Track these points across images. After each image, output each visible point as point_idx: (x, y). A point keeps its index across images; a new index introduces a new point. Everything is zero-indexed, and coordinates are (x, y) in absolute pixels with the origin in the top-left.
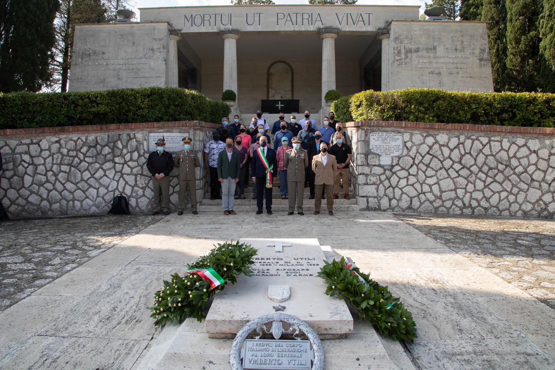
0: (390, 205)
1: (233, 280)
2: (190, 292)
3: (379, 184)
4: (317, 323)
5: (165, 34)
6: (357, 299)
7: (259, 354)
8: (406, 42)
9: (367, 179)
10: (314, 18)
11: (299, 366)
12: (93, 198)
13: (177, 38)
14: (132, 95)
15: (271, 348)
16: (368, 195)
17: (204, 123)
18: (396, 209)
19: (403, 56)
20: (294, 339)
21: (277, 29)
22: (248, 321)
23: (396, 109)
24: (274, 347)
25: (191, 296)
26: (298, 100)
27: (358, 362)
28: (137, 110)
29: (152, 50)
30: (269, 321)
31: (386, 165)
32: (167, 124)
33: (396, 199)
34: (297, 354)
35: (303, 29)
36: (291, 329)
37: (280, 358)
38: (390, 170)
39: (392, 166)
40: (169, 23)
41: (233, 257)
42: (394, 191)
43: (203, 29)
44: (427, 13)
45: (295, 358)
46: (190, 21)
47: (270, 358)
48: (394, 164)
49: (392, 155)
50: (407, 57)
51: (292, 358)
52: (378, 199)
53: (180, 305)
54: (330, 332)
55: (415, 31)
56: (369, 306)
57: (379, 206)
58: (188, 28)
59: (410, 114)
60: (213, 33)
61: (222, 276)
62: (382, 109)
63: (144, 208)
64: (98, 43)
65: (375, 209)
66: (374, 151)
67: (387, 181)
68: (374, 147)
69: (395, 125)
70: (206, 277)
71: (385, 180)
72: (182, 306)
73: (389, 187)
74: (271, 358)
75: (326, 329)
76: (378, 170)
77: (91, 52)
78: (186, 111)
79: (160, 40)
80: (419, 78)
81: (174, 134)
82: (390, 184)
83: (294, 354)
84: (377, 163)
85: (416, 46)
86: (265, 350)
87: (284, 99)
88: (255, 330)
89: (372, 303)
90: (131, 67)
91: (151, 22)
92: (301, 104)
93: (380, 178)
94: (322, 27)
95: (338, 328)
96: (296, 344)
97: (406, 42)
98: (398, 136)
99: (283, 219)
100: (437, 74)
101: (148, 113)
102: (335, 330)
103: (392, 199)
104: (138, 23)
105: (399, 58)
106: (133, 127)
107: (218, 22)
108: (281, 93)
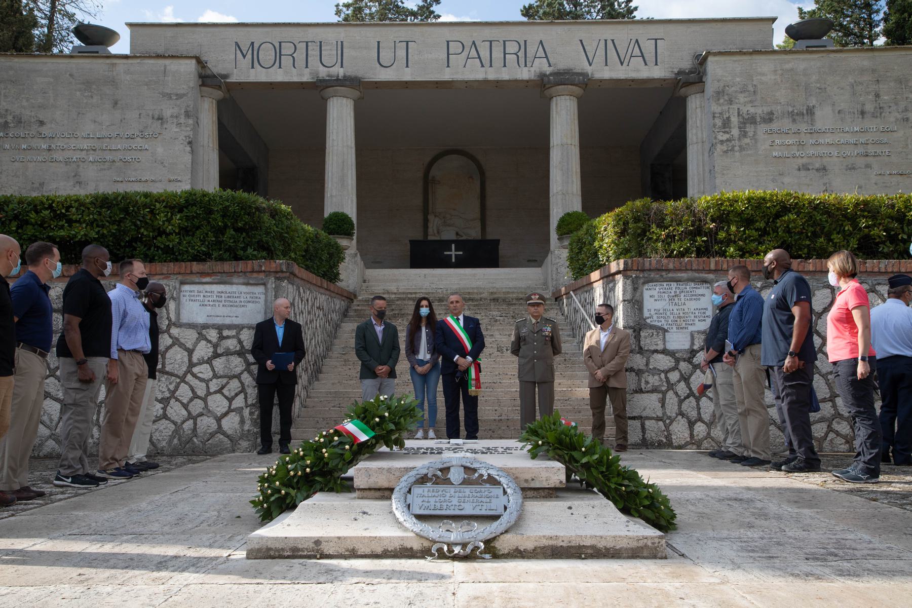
0: (692, 435)
3: (667, 391)
4: (514, 471)
5: (192, 84)
6: (575, 454)
7: (432, 500)
8: (742, 100)
9: (639, 380)
10: (531, 51)
12: (51, 420)
13: (219, 94)
14: (145, 206)
16: (644, 414)
18: (705, 444)
19: (735, 132)
21: (447, 75)
23: (700, 234)
24: (452, 493)
26: (497, 242)
27: (571, 511)
28: (155, 238)
29: (160, 118)
30: (445, 466)
31: (678, 351)
33: (703, 422)
34: (484, 500)
35: (505, 75)
36: (476, 475)
38: (689, 361)
39: (693, 352)
40: (199, 61)
42: (698, 405)
43: (278, 76)
44: (791, 31)
46: (249, 56)
48: (695, 348)
49: (691, 328)
50: (744, 134)
52: (664, 422)
54: (533, 485)
55: (763, 74)
57: (669, 437)
58: (244, 73)
59: (728, 246)
60: (302, 83)
61: (373, 430)
62: (668, 236)
63: (164, 444)
64: (27, 100)
65: (660, 445)
66: (654, 321)
68: (653, 312)
70: (348, 433)
71: (679, 381)
73: (687, 397)
75: (526, 481)
76: (663, 362)
77: (9, 118)
78: (258, 242)
79: (180, 96)
80: (773, 181)
81: (234, 288)
82: (690, 389)
83: (480, 499)
84: (660, 347)
85: (766, 109)
87: (464, 238)
88: (426, 475)
89: (596, 456)
90: (108, 158)
91: (159, 57)
92: (503, 249)
93: (667, 378)
94: (548, 70)
97: (742, 100)
98: (702, 290)
100: (817, 170)
101: (179, 243)
103: (696, 421)
104: (126, 57)
105: (726, 137)
107: (314, 61)
108: (456, 223)
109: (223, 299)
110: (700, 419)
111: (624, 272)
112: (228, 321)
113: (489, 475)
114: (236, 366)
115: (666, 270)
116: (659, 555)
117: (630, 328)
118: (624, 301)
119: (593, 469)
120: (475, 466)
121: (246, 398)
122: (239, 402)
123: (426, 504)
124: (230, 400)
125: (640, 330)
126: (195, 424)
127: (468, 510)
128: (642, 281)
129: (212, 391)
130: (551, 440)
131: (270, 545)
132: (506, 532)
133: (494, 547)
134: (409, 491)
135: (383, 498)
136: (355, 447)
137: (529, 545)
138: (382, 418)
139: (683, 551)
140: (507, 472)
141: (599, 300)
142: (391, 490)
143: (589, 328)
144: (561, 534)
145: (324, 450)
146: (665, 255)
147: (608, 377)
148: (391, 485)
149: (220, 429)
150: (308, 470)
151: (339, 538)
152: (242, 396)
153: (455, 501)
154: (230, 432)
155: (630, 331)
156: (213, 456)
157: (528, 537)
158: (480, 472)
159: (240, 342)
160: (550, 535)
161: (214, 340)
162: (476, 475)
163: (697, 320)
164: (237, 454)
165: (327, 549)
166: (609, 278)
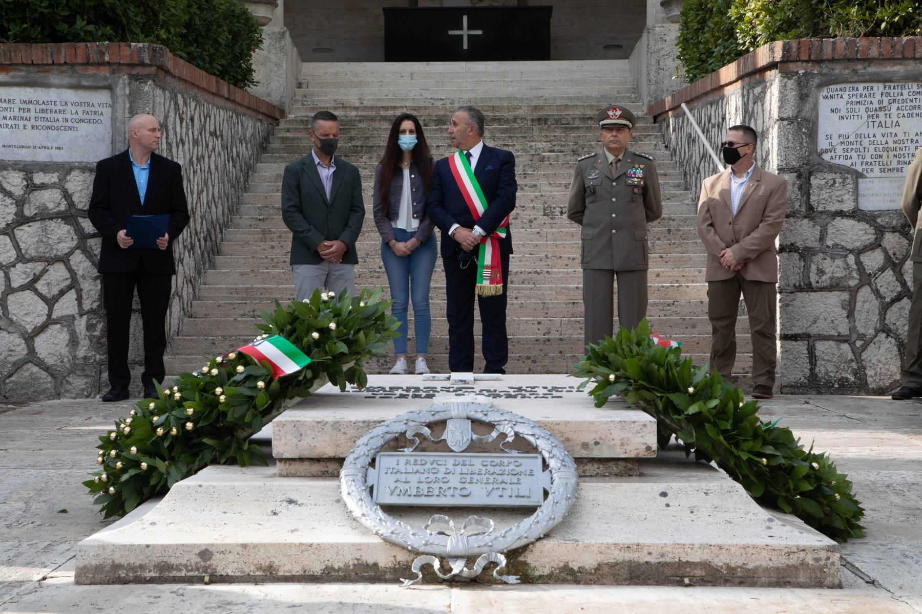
2: (219, 390)
4: (562, 428)
7: (414, 479)
9: (807, 268)
16: (814, 330)
17: (169, 59)
20: (502, 451)
25: (222, 398)
27: (665, 500)
30: (437, 417)
31: (881, 213)
36: (494, 434)
37: (467, 486)
45: (503, 485)
47: (442, 485)
51: (495, 486)
54: (596, 453)
57: (860, 372)
61: (308, 353)
65: (844, 388)
67: (889, 273)
68: (835, 141)
70: (263, 358)
71: (882, 270)
72: (195, 430)
73: (898, 299)
75: (585, 446)
76: (853, 233)
81: (53, 94)
83: (500, 478)
84: (848, 206)
88: (403, 434)
89: (714, 403)
93: (859, 263)
95: (618, 443)
96: (506, 461)
102: (610, 447)
111: (782, 65)
112: (42, 156)
113: (517, 434)
114: (60, 240)
116: (828, 581)
117: (791, 170)
119: (707, 425)
120: (491, 418)
121: (79, 299)
122: (67, 306)
123: (402, 486)
124: (51, 302)
125: (810, 174)
127: (479, 497)
128: (817, 81)
129: (15, 285)
130: (631, 372)
132: (547, 536)
133: (525, 564)
134: (372, 463)
137: (589, 561)
138: (324, 331)
139: (873, 575)
140: (550, 429)
142: (340, 461)
145: (219, 390)
148: (339, 453)
149: (32, 356)
150: (189, 425)
151: (245, 546)
152: (72, 295)
153: (455, 481)
154: (50, 361)
157: (587, 546)
159: (67, 196)
160: (627, 542)
161: (18, 191)
162: (494, 434)
164: (65, 400)
165: (224, 566)
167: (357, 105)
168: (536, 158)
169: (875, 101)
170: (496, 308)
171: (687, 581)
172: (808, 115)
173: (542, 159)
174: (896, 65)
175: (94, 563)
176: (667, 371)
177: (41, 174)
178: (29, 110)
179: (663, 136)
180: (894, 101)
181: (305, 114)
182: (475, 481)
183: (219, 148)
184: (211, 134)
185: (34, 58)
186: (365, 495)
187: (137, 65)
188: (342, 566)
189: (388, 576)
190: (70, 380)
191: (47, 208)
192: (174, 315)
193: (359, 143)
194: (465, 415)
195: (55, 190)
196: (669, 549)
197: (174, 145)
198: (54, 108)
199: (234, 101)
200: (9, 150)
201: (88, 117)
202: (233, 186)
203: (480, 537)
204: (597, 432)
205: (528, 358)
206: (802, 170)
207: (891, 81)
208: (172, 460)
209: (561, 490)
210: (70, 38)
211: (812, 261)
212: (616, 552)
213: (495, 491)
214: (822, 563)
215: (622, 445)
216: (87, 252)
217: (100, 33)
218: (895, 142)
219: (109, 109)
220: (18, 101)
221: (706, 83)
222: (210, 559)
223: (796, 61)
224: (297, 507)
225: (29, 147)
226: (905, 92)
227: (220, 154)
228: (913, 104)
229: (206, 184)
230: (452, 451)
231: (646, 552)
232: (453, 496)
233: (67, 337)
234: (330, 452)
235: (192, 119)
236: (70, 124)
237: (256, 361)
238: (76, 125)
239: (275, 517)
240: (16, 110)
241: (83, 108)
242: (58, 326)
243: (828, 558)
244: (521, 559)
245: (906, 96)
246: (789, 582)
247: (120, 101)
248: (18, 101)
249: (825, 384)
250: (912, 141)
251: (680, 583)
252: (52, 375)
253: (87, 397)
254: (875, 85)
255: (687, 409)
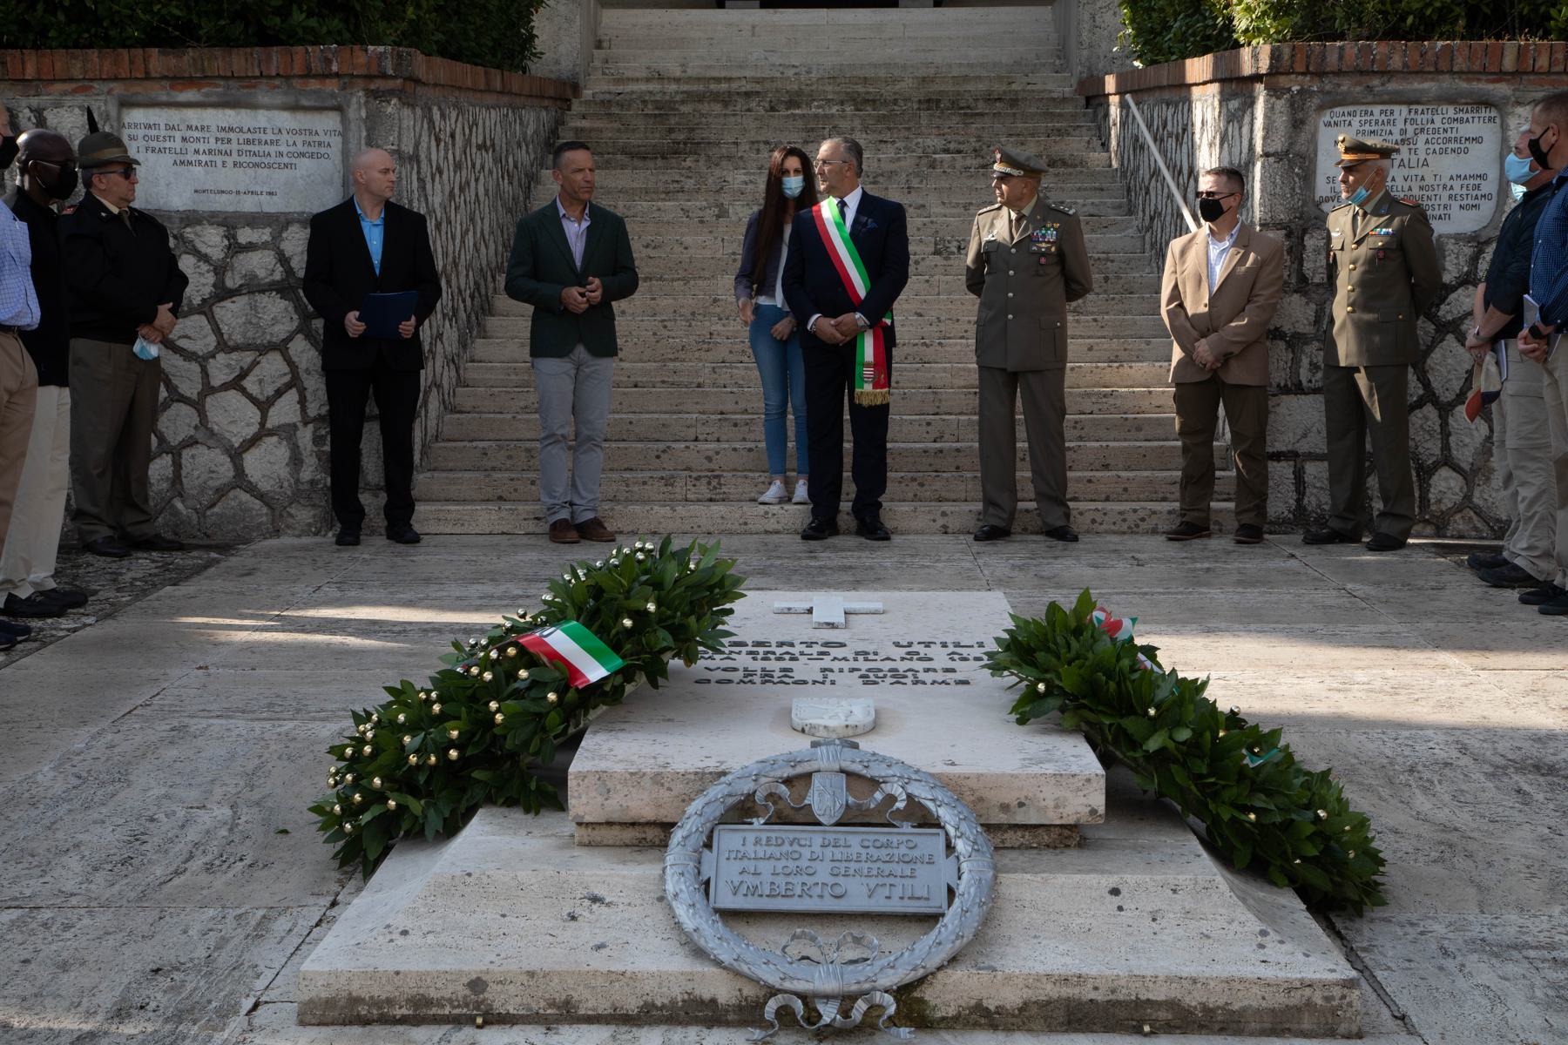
1: (656, 672)
4: (972, 783)
6: (1130, 724)
7: (766, 867)
9: (1296, 362)
11: (906, 902)
15: (806, 853)
16: (1303, 447)
17: (420, 63)
18: (1458, 523)
22: (724, 774)
24: (817, 848)
25: (499, 717)
27: (1116, 900)
30: (799, 770)
32: (218, 61)
33: (1457, 469)
34: (897, 868)
36: (878, 796)
37: (840, 880)
41: (657, 585)
42: (1444, 424)
45: (891, 880)
47: (805, 878)
51: (880, 881)
53: (453, 754)
54: (1020, 819)
56: (1171, 745)
61: (616, 647)
69: (1460, 63)
70: (554, 656)
74: (810, 881)
75: (1005, 808)
81: (261, 118)
83: (887, 868)
86: (787, 856)
88: (751, 796)
89: (1184, 735)
95: (1050, 803)
96: (895, 839)
98: (1479, 126)
99: (846, 562)
102: (1039, 810)
106: (30, 72)
109: (234, 146)
110: (1447, 461)
111: (1271, 80)
112: (248, 205)
113: (910, 797)
114: (275, 321)
115: (1382, 73)
116: (1342, 1028)
117: (1278, 226)
118: (1266, 155)
119: (1174, 768)
120: (876, 771)
121: (302, 401)
122: (285, 411)
123: (750, 880)
124: (264, 406)
125: (1305, 231)
126: (177, 465)
127: (857, 901)
128: (1316, 101)
129: (216, 382)
130: (1067, 684)
131: (356, 989)
132: (953, 960)
133: (921, 1001)
134: (708, 845)
135: (641, 846)
136: (571, 695)
137: (1011, 997)
138: (640, 616)
139: (1405, 1003)
140: (954, 787)
141: (1207, 158)
142: (668, 827)
143: (1181, 229)
144: (1092, 969)
145: (493, 705)
146: (1381, 26)
147: (1226, 358)
148: (666, 815)
149: (240, 479)
150: (453, 754)
151: (531, 974)
152: (292, 396)
153: (823, 873)
154: (264, 486)
155: (1276, 236)
156: (225, 548)
157: (1008, 978)
158: (887, 788)
159: (283, 259)
160: (1063, 971)
161: (217, 253)
162: (878, 796)
163: (1455, 205)
164: (286, 540)
165: (504, 1000)
166: (1236, 87)
167: (678, 74)
168: (924, 161)
169: (1396, 130)
170: (874, 420)
171: (1147, 1028)
172: (1304, 149)
173: (932, 165)
174: (1426, 80)
175: (324, 995)
176: (1118, 684)
177: (248, 230)
178: (229, 141)
179: (1099, 128)
180: (1422, 130)
181: (605, 88)
182: (852, 872)
183: (489, 163)
184: (479, 147)
185: (235, 68)
186: (699, 897)
187: (376, 77)
188: (666, 1001)
189: (731, 1017)
190: (293, 511)
191: (256, 276)
192: (430, 417)
193: (681, 137)
194: (837, 767)
195: (266, 252)
196: (1123, 982)
197: (429, 179)
198: (263, 137)
199: (510, 93)
200: (203, 196)
201: (311, 150)
202: (509, 211)
203: (860, 967)
204: (1021, 789)
205: (914, 480)
206: (1293, 226)
207: (1418, 103)
208: (430, 794)
209: (972, 890)
210: (283, 37)
211: (1303, 351)
212: (1049, 987)
213: (880, 890)
214: (1335, 1003)
215: (1057, 806)
216: (309, 336)
217: (324, 29)
218: (1421, 188)
219: (339, 139)
220: (214, 128)
221: (1163, 74)
222: (484, 991)
223: (1288, 73)
224: (603, 907)
225: (230, 192)
226: (1438, 119)
227: (491, 172)
228: (1449, 135)
229: (472, 220)
230: (820, 824)
231: (1090, 986)
232: (821, 897)
233: (288, 454)
234: (648, 814)
235: (453, 136)
236: (286, 160)
237: (545, 659)
238: (293, 161)
239: (573, 924)
240: (212, 140)
241: (303, 138)
242: (275, 439)
243: (1344, 997)
244: (916, 994)
245: (1438, 124)
246: (1289, 1030)
247: (353, 126)
248: (214, 128)
249: (1316, 520)
250: (1445, 187)
251: (1138, 1031)
252: (267, 505)
253: (316, 534)
254: (1396, 108)
255: (1147, 738)
